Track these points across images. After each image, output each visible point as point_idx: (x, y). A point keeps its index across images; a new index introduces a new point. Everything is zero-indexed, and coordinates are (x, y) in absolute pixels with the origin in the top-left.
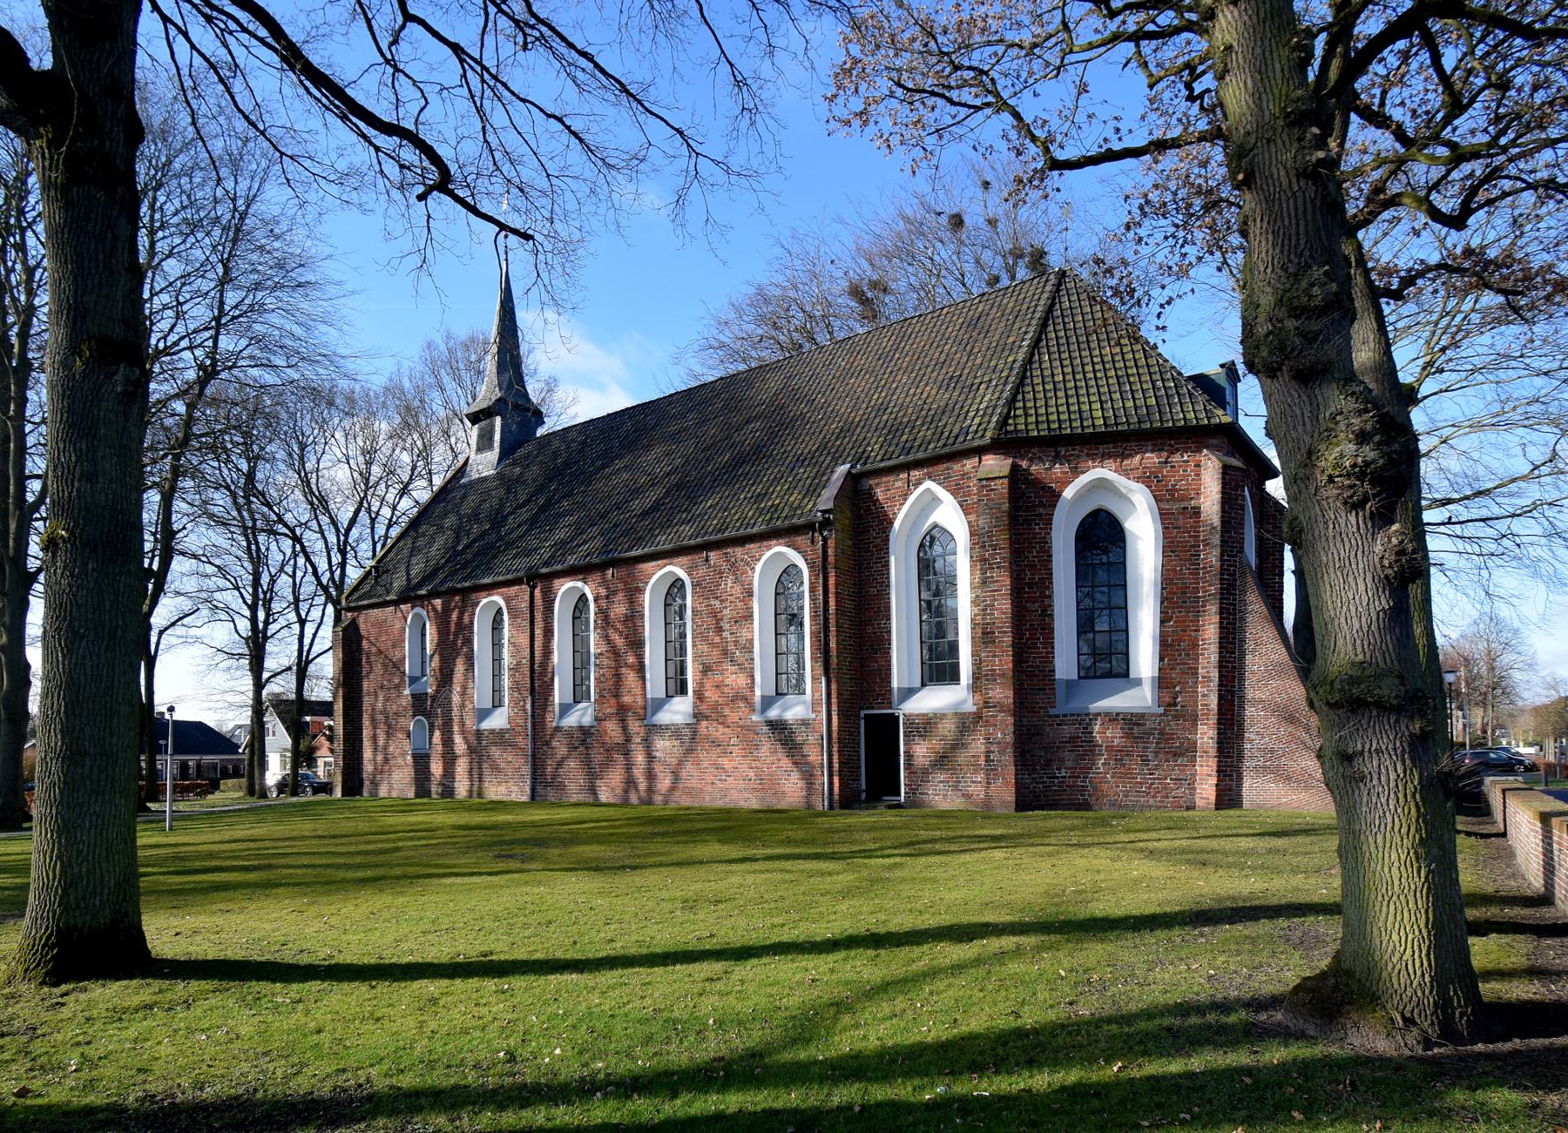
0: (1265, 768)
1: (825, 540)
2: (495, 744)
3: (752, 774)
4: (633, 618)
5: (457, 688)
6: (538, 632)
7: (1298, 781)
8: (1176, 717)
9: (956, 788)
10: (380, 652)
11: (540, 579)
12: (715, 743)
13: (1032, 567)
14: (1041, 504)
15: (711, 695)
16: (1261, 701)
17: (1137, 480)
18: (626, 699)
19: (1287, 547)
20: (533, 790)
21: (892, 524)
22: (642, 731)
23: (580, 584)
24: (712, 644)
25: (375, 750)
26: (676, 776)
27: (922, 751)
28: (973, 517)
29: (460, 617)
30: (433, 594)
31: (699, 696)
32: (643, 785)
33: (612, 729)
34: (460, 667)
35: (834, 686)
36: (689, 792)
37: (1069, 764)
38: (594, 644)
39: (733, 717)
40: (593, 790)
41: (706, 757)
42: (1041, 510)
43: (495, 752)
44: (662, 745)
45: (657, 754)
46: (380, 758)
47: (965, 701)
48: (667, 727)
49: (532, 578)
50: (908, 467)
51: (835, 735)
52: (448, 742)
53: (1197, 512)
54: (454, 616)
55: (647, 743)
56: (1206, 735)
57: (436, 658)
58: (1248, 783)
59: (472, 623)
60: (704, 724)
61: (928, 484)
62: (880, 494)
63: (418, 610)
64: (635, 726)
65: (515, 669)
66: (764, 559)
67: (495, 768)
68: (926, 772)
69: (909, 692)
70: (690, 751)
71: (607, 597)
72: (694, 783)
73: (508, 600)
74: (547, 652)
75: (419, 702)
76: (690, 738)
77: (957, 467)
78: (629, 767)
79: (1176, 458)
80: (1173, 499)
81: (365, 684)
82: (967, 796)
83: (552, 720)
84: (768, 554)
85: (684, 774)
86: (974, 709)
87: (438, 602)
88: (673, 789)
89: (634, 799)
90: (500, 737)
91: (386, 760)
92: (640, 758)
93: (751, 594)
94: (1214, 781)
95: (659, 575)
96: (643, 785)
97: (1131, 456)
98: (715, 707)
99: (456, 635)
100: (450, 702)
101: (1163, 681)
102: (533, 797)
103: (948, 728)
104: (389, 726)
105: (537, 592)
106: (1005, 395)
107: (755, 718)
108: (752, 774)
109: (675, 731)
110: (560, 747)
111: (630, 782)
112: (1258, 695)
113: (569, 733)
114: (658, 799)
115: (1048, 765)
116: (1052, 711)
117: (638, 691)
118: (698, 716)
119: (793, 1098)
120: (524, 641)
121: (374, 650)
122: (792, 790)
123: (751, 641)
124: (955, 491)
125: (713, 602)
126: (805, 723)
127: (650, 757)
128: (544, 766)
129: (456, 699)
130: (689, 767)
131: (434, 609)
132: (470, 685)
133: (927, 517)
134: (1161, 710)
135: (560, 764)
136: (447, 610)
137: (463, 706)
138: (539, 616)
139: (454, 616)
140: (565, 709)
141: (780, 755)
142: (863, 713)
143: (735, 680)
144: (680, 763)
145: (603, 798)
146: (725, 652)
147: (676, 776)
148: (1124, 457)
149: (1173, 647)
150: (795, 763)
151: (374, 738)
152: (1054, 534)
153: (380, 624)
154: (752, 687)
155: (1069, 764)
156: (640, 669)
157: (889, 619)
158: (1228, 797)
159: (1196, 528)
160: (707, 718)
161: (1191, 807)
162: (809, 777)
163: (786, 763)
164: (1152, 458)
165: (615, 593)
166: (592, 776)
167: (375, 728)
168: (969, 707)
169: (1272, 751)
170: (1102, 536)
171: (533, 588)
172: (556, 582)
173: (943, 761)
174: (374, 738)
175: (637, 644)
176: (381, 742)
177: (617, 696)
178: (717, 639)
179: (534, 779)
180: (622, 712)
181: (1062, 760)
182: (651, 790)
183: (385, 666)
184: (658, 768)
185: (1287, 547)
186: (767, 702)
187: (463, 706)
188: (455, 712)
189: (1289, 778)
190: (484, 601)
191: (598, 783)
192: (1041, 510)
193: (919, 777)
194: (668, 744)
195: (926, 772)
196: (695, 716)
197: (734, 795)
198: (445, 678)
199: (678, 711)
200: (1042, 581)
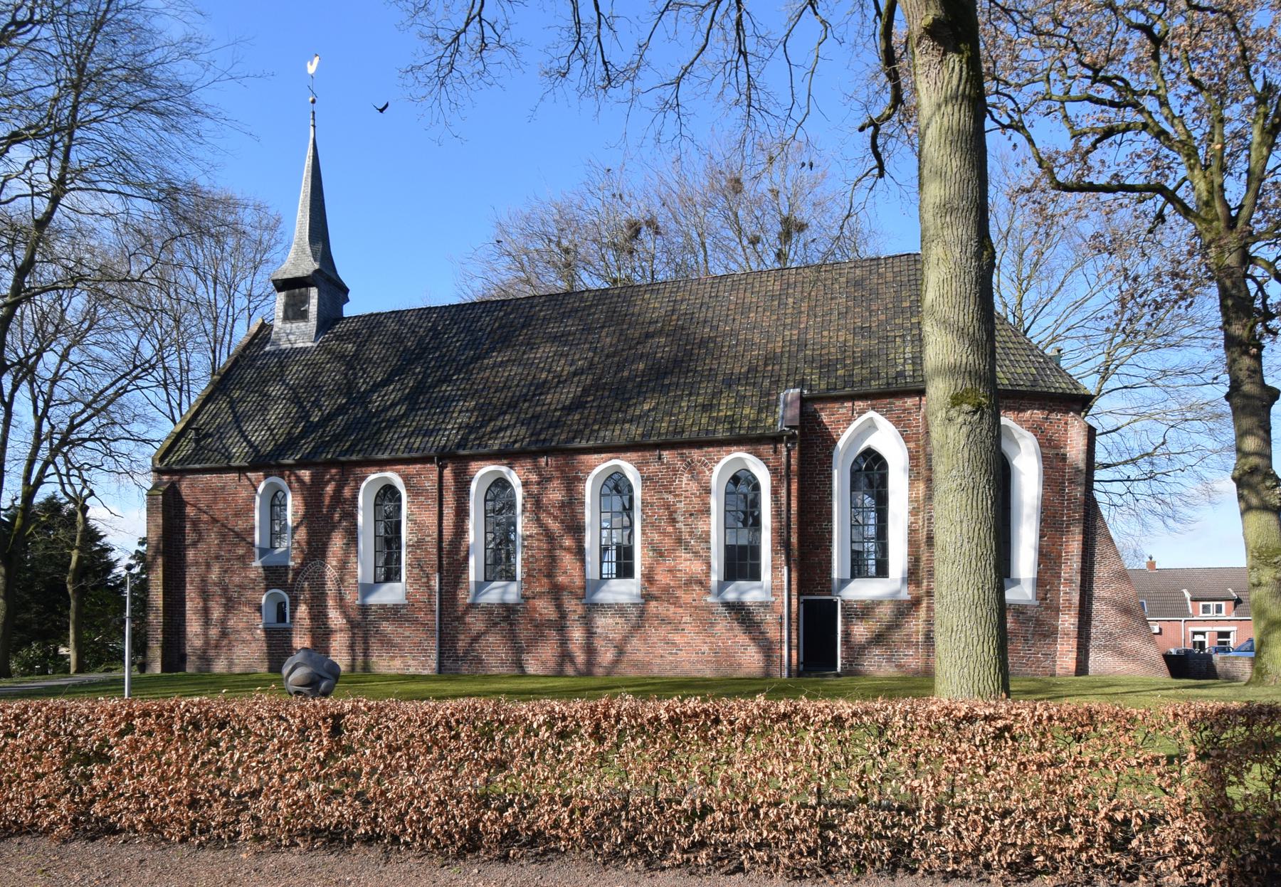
0: (1105, 646)
1: (789, 451)
2: (387, 619)
3: (705, 648)
4: (572, 504)
5: (332, 562)
6: (449, 513)
7: (1128, 656)
8: (1046, 609)
9: (889, 660)
10: (215, 521)
11: (456, 459)
12: (664, 621)
15: (662, 578)
16: (1104, 599)
17: (1029, 429)
18: (561, 579)
20: (440, 664)
21: (835, 442)
22: (580, 610)
23: (504, 469)
24: (664, 533)
25: (207, 622)
26: (621, 651)
27: (861, 631)
28: (912, 445)
29: (338, 490)
30: (302, 464)
31: (649, 578)
32: (580, 658)
33: (545, 608)
34: (337, 543)
35: (794, 575)
36: (635, 665)
38: (522, 525)
39: (685, 597)
40: (519, 664)
41: (656, 633)
43: (387, 627)
44: (604, 623)
45: (598, 630)
46: (214, 632)
47: (899, 592)
48: (610, 606)
49: (443, 457)
50: (853, 398)
51: (794, 616)
52: (318, 615)
53: (1064, 458)
54: (330, 489)
55: (587, 623)
56: (1068, 621)
57: (302, 534)
58: (1092, 656)
59: (355, 498)
60: (653, 604)
61: (871, 414)
62: (825, 417)
63: (274, 479)
64: (573, 606)
65: (417, 545)
66: (723, 462)
67: (387, 643)
68: (863, 648)
69: (844, 583)
70: (637, 627)
71: (539, 483)
72: (640, 656)
73: (407, 479)
74: (460, 531)
75: (275, 575)
76: (639, 617)
77: (899, 403)
78: (564, 642)
79: (1053, 416)
80: (1050, 446)
81: (190, 554)
82: (899, 666)
83: (464, 597)
84: (727, 459)
85: (629, 648)
86: (909, 597)
87: (306, 474)
88: (616, 662)
89: (569, 670)
90: (393, 613)
91: (224, 634)
92: (577, 634)
93: (708, 491)
94: (1074, 655)
95: (599, 467)
96: (580, 658)
97: (1024, 411)
98: (666, 589)
99: (332, 508)
100: (322, 575)
101: (1040, 582)
102: (441, 667)
103: (885, 613)
104: (229, 599)
105: (448, 473)
107: (710, 599)
108: (705, 648)
109: (620, 610)
110: (476, 623)
111: (566, 655)
112: (1102, 594)
113: (489, 609)
114: (599, 671)
117: (576, 573)
118: (647, 597)
120: (430, 518)
121: (205, 517)
122: (750, 659)
123: (708, 533)
124: (897, 422)
125: (666, 496)
126: (764, 605)
127: (590, 633)
128: (454, 640)
129: (331, 572)
130: (635, 642)
131: (299, 480)
132: (353, 559)
133: (863, 441)
134: (1037, 603)
135: (476, 639)
136: (318, 483)
137: (341, 580)
138: (449, 499)
139: (330, 489)
140: (480, 587)
141: (736, 632)
143: (688, 565)
144: (626, 639)
145: (531, 669)
146: (679, 540)
147: (621, 651)
148: (1020, 411)
149: (1048, 559)
150: (753, 639)
151: (206, 612)
153: (216, 493)
154: (708, 574)
156: (580, 552)
157: (830, 520)
158: (1082, 668)
159: (1063, 470)
160: (656, 598)
161: (1053, 675)
162: (768, 649)
163: (743, 639)
164: (1038, 414)
165: (549, 479)
166: (518, 654)
167: (206, 600)
168: (905, 595)
169: (1111, 634)
170: (871, 469)
171: (442, 468)
172: (473, 465)
173: (879, 639)
174: (206, 612)
175: (577, 530)
176: (216, 614)
177: (550, 575)
178: (670, 529)
179: (441, 654)
180: (556, 592)
182: (590, 663)
183: (223, 537)
184: (599, 644)
186: (721, 587)
187: (341, 580)
188: (330, 586)
189: (1122, 653)
190: (372, 477)
191: (524, 656)
193: (856, 652)
194: (611, 621)
195: (863, 648)
196: (643, 596)
197: (687, 666)
198: (316, 550)
199: (623, 591)
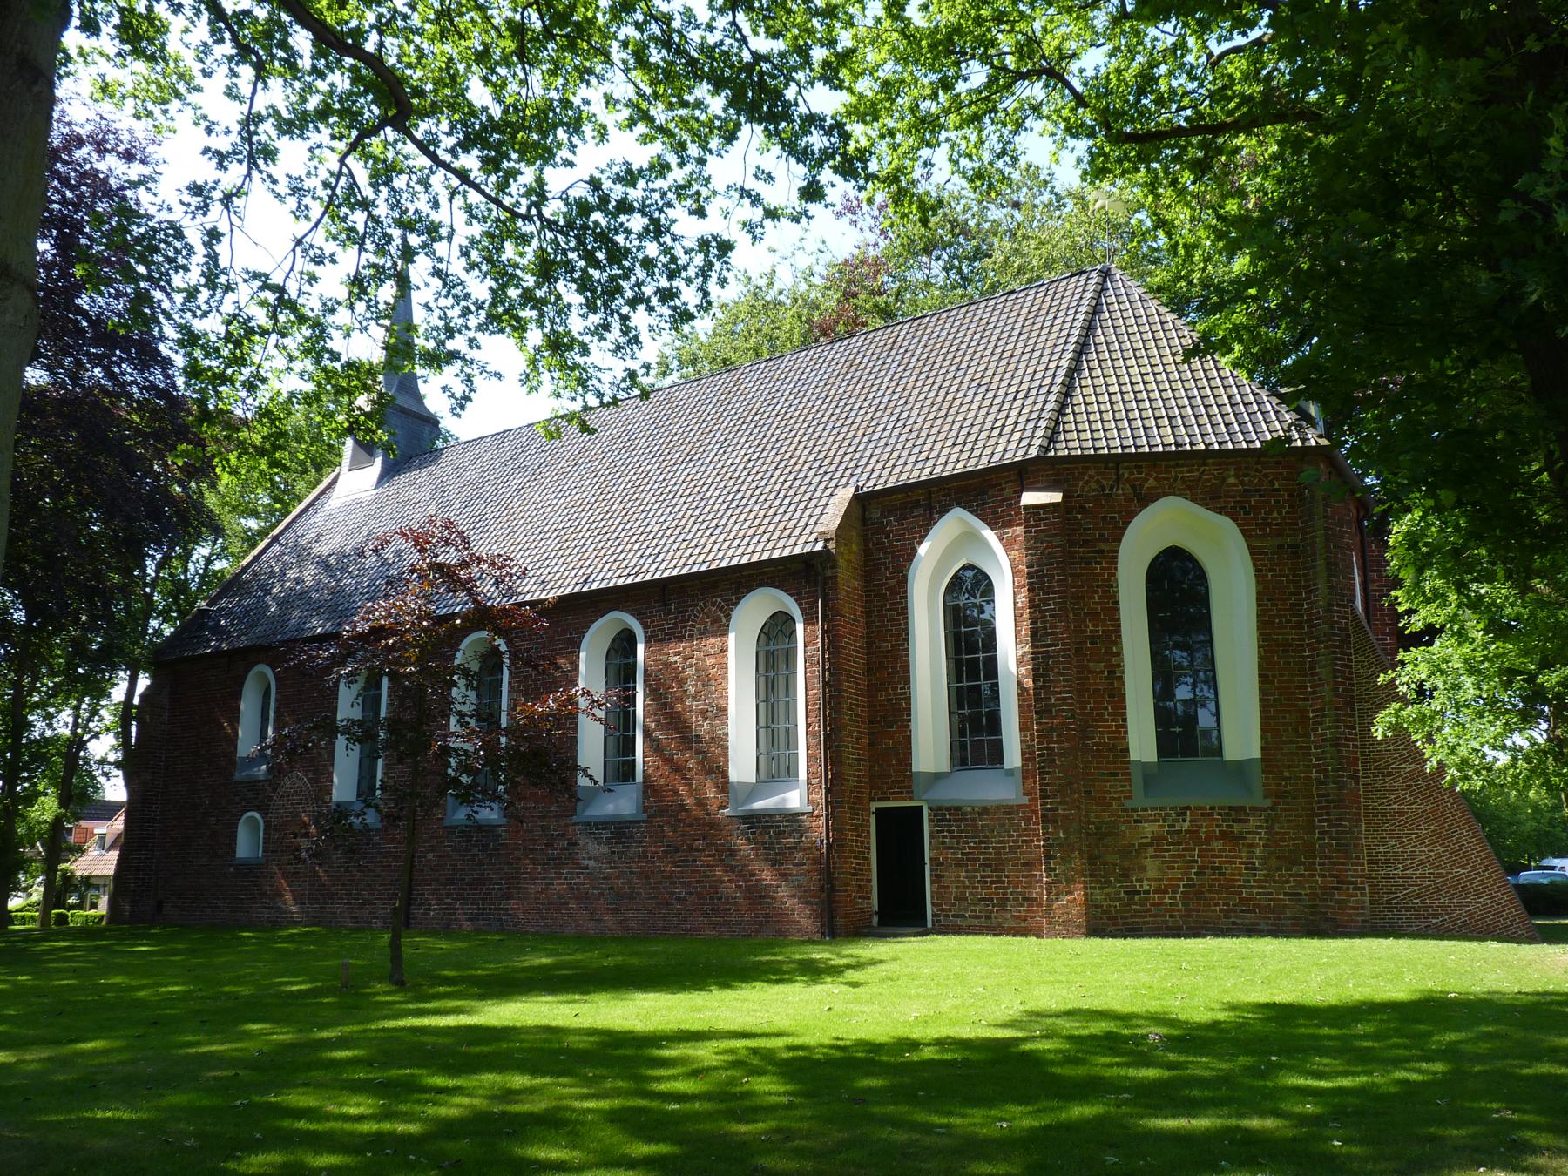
13: (1094, 616)
14: (1102, 538)
19: (1056, 497)
37: (1152, 874)
42: (1103, 546)
106: (1050, 406)
115: (1125, 875)
116: (1128, 804)
119: (654, 1104)
142: (874, 806)
152: (1119, 574)
155: (1152, 874)
181: (1144, 869)
185: (1056, 497)
192: (1103, 546)
200: (1108, 634)
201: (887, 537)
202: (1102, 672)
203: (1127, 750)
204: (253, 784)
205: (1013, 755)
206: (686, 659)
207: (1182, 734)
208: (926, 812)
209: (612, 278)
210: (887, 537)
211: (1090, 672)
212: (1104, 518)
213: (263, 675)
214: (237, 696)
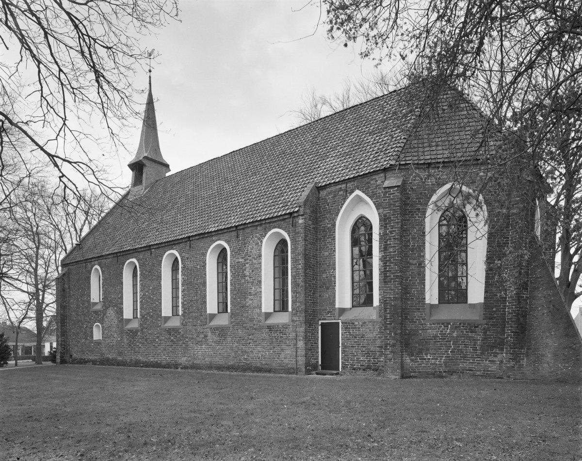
42: (419, 206)
192: (419, 206)
200: (419, 247)
201: (328, 205)
202: (416, 264)
203: (425, 299)
204: (96, 312)
205: (376, 302)
206: (245, 260)
207: (453, 290)
208: (340, 324)
209: (469, 194)
210: (328, 205)
211: (411, 264)
212: (421, 193)
213: (96, 269)
214: (89, 278)
